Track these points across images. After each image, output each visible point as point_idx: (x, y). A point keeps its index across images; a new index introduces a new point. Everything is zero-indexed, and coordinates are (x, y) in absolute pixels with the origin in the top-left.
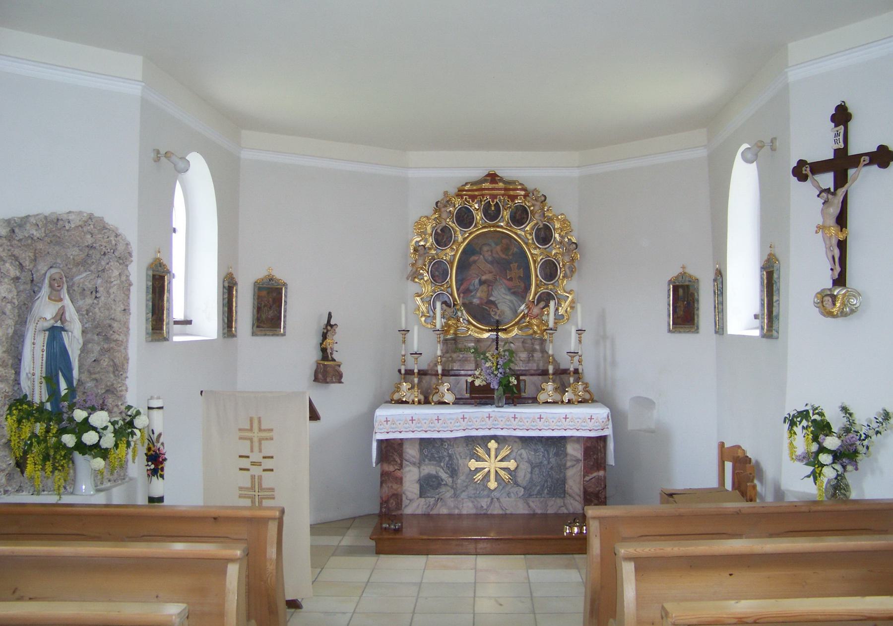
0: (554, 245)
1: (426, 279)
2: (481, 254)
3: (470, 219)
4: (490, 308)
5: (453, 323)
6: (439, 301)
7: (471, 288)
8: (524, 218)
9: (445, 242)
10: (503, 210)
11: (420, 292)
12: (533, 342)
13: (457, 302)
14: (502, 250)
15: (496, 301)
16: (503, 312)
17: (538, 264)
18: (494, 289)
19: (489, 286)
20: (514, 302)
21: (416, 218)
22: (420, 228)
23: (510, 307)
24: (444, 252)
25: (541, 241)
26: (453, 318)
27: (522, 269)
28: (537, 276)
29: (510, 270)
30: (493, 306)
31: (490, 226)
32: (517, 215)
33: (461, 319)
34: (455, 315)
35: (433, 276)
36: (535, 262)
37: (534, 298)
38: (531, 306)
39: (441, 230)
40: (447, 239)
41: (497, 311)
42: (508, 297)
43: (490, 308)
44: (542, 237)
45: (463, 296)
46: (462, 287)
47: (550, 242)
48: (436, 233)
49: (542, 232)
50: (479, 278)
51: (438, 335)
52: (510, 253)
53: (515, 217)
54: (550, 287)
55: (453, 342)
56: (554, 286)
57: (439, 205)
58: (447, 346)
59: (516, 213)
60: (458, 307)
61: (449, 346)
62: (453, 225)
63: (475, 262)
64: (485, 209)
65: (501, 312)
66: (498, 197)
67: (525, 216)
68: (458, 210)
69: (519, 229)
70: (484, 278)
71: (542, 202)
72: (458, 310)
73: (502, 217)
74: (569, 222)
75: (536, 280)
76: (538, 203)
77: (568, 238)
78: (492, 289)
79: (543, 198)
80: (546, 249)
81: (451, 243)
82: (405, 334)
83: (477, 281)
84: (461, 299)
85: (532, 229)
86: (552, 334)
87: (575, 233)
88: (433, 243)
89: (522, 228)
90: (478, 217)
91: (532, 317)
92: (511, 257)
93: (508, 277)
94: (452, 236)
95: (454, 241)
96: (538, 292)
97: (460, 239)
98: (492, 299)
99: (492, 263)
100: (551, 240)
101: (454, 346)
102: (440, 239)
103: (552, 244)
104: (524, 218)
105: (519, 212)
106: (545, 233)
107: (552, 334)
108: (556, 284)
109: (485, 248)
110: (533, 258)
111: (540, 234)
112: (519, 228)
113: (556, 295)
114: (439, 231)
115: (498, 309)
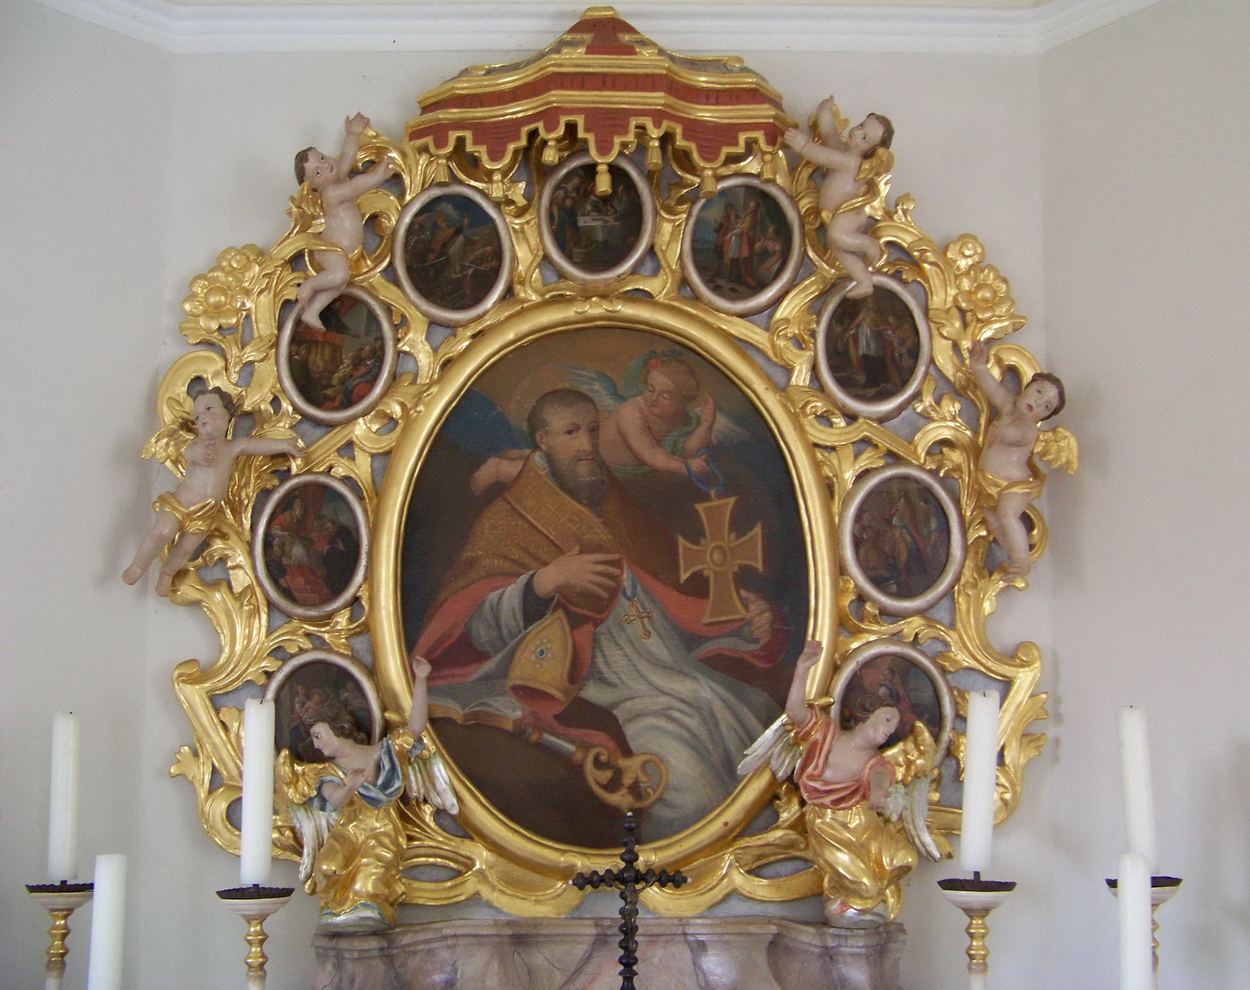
0: (928, 400)
1: (241, 579)
2: (536, 447)
3: (480, 260)
4: (585, 747)
5: (376, 837)
6: (796, 796)
7: (482, 633)
8: (765, 254)
9: (343, 382)
10: (656, 213)
11: (203, 655)
12: (831, 943)
13: (399, 709)
14: (648, 429)
15: (616, 704)
16: (654, 764)
17: (845, 503)
18: (605, 642)
19: (576, 622)
20: (724, 716)
21: (198, 260)
22: (218, 306)
23: (694, 744)
24: (337, 438)
25: (861, 378)
26: (374, 802)
27: (758, 530)
28: (840, 570)
29: (696, 534)
30: (598, 737)
31: (586, 295)
32: (732, 239)
33: (428, 809)
34: (386, 785)
35: (276, 569)
36: (828, 488)
37: (826, 691)
38: (816, 735)
39: (325, 315)
40: (357, 362)
41: (623, 763)
42: (684, 687)
43: (585, 747)
44: (866, 357)
45: (430, 678)
46: (431, 633)
47: (905, 383)
48: (302, 335)
49: (866, 331)
50: (523, 579)
51: (249, 919)
52: (694, 442)
53: (719, 250)
54: (913, 626)
55: (373, 944)
56: (931, 623)
57: (310, 166)
58: (339, 966)
59: (722, 228)
60: (401, 741)
61: (349, 966)
62: (389, 293)
63: (499, 489)
64: (562, 208)
65: (644, 766)
66: (633, 122)
67: (777, 247)
68: (417, 215)
69: (742, 316)
70: (548, 579)
71: (868, 155)
72: (406, 757)
73: (651, 251)
74: (1005, 281)
75: (838, 592)
76: (851, 161)
77: (999, 361)
78: (595, 642)
79: (877, 132)
80: (881, 420)
81: (378, 390)
82: (70, 911)
83: (511, 595)
84: (421, 688)
85: (815, 308)
86: (985, 911)
87: (1034, 339)
88: (283, 390)
89: (759, 311)
90: (523, 253)
91: (827, 800)
92: (697, 464)
93: (684, 576)
94: (382, 348)
95: (394, 377)
96: (846, 657)
97: (425, 359)
98: (593, 693)
99: (592, 498)
100: (912, 371)
101: (379, 966)
102: (318, 361)
103: (917, 396)
104: (765, 254)
105: (745, 224)
106: (878, 335)
107: (985, 911)
108: (942, 613)
109: (558, 418)
110: (817, 466)
111: (856, 338)
112: (741, 306)
113: (944, 671)
114: (312, 318)
115: (627, 752)
